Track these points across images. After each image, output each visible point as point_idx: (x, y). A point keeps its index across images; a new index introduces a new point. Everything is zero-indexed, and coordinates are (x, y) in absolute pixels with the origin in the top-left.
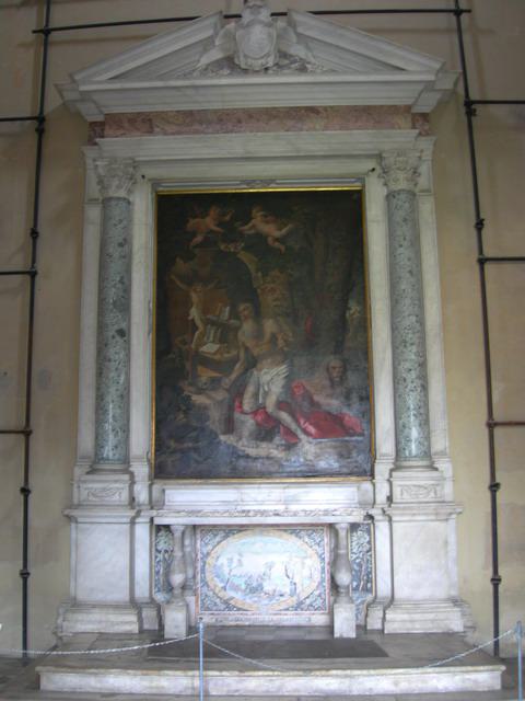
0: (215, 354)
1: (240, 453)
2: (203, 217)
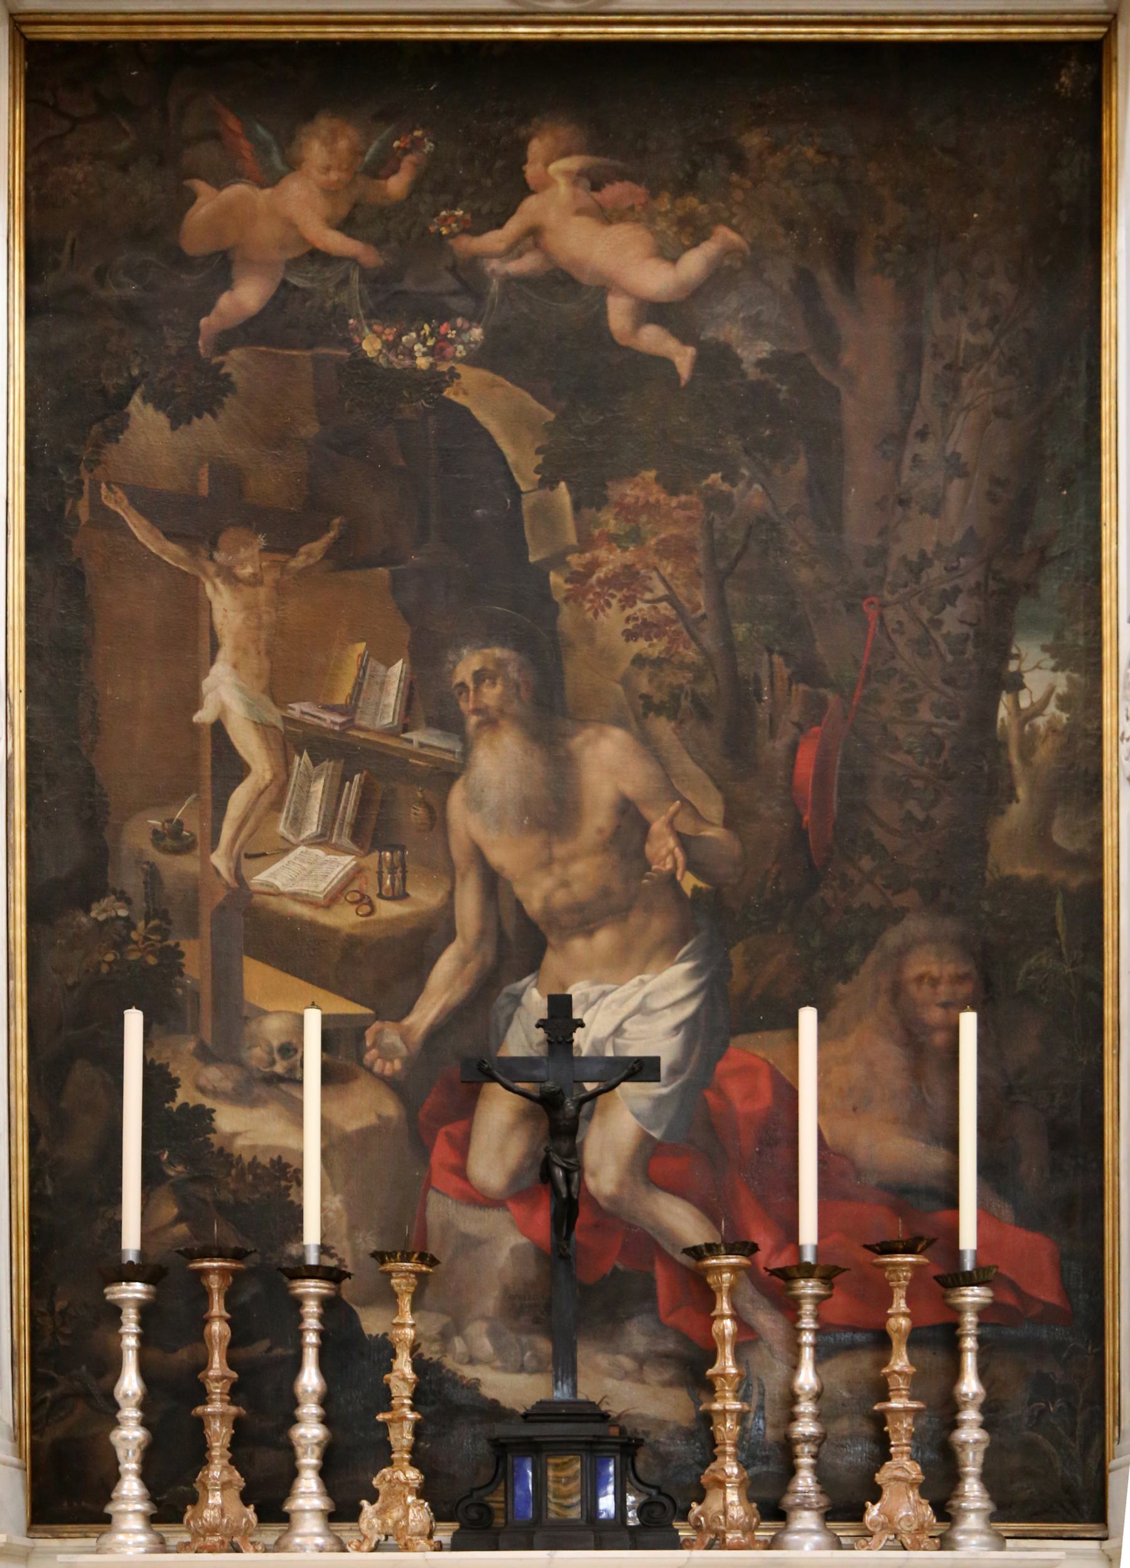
0: (333, 899)
1: (460, 1397)
2: (269, 179)
